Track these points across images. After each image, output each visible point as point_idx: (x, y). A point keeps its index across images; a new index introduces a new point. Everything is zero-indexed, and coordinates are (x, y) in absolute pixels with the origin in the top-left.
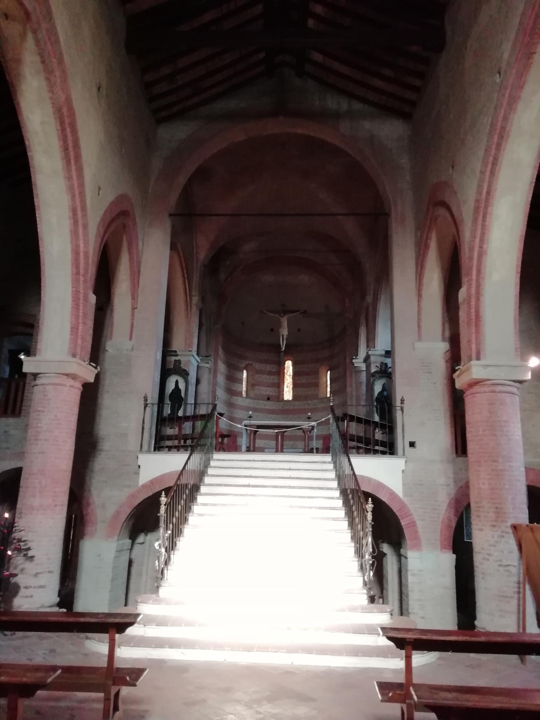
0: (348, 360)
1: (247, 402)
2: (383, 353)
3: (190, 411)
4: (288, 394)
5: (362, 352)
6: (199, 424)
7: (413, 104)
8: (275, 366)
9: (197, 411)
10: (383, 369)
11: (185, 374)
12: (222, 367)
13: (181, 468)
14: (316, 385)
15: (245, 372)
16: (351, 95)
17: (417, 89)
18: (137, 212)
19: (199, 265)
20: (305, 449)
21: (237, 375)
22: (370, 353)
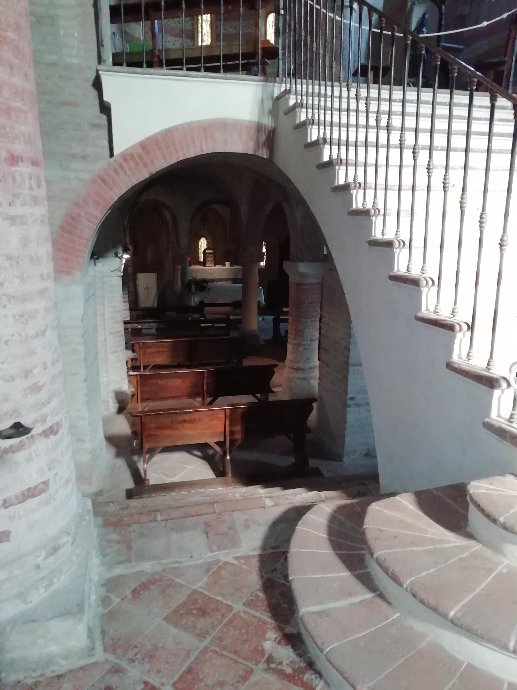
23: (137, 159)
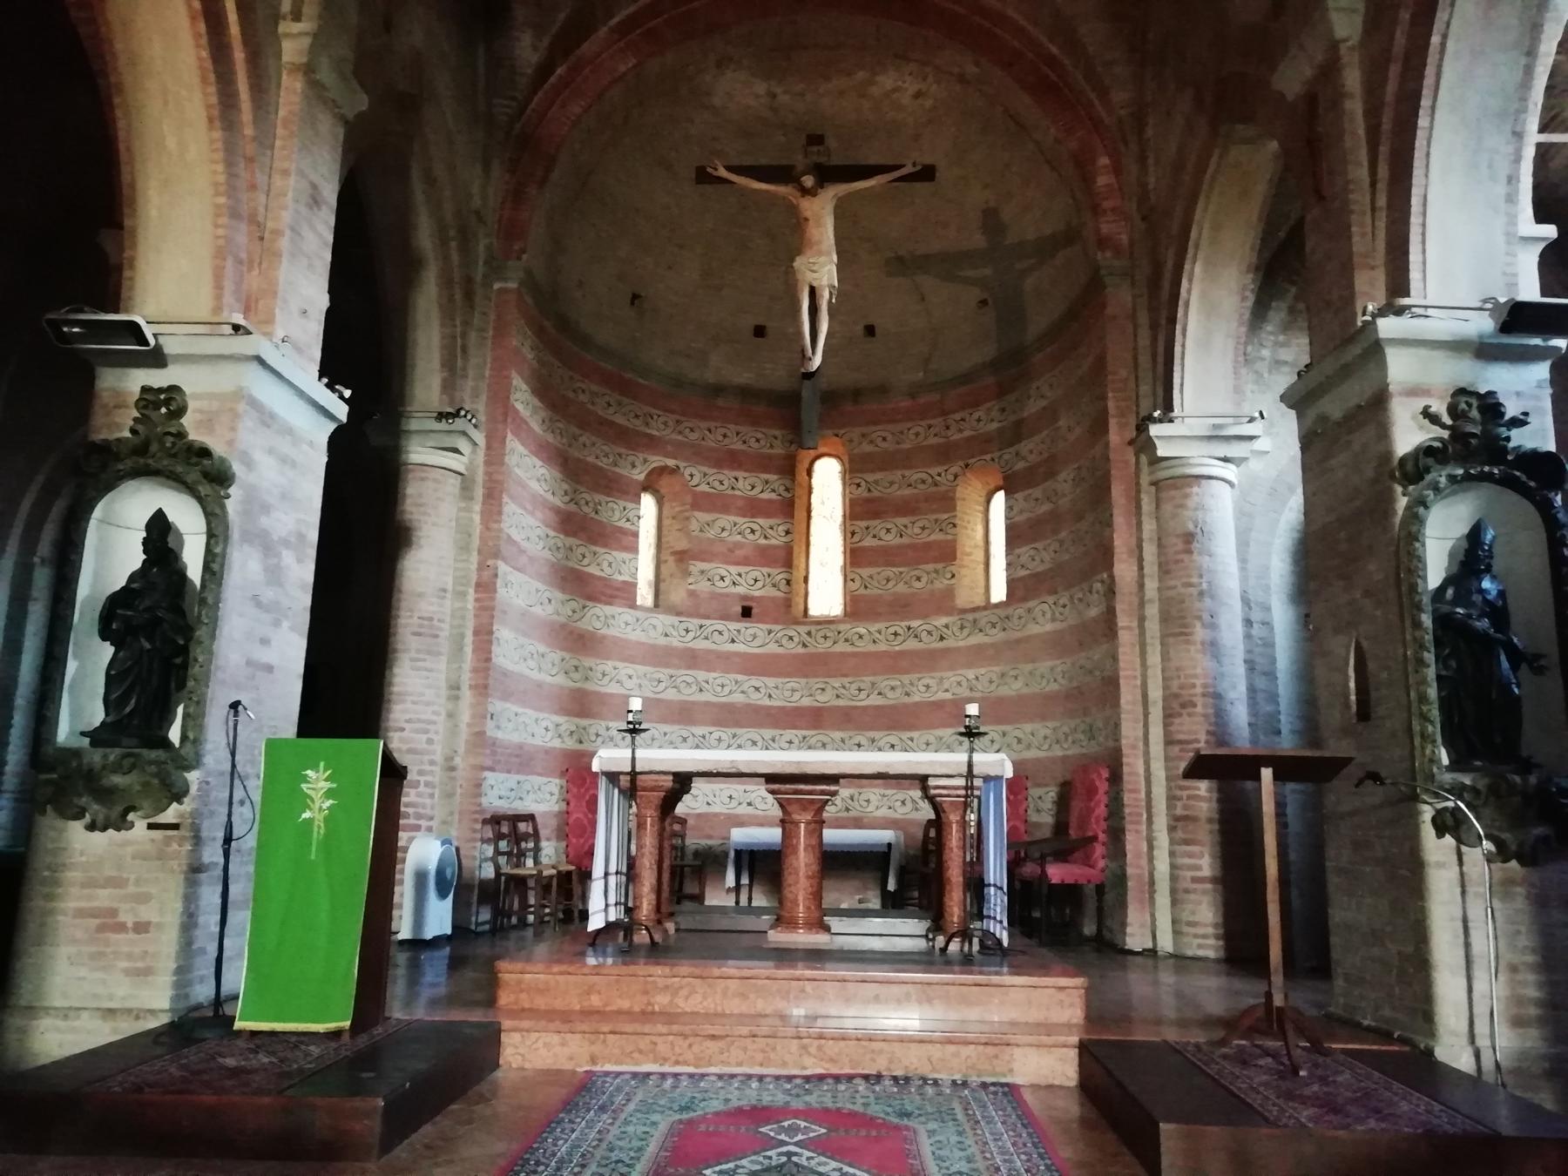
0: (1116, 435)
1: (660, 629)
2: (1483, 325)
4: (826, 592)
8: (772, 477)
12: (531, 474)
14: (947, 554)
15: (648, 503)
21: (612, 512)
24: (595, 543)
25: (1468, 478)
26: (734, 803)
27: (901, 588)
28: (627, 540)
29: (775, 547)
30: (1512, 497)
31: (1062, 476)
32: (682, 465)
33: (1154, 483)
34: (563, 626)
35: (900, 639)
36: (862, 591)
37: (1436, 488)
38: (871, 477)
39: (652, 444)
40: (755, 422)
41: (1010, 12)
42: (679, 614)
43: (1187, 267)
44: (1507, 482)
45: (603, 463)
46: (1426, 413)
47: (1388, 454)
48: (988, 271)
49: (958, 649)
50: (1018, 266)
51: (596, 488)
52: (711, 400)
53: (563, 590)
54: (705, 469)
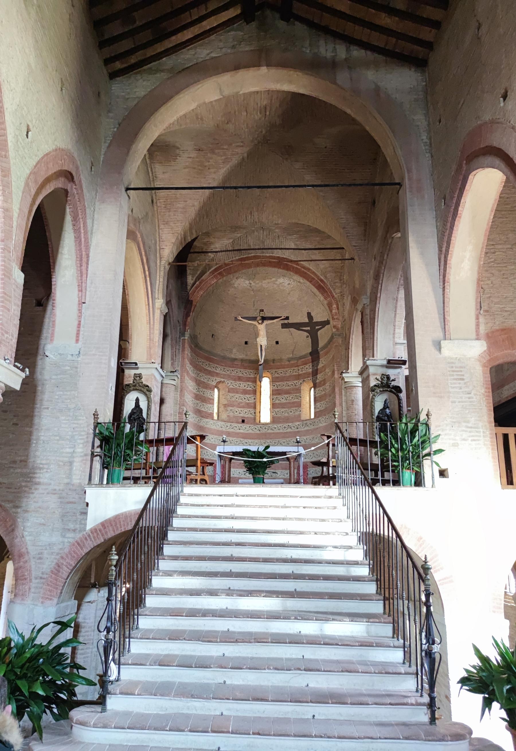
2: (385, 362)
3: (152, 435)
4: (265, 415)
5: (356, 363)
6: (166, 450)
7: (429, 46)
9: (162, 432)
10: (385, 382)
11: (146, 390)
12: (190, 385)
13: (142, 506)
14: (299, 405)
16: (350, 41)
17: (436, 25)
18: (84, 177)
19: (163, 262)
20: (290, 479)
21: (207, 393)
22: (368, 363)
23: (99, 532)
24: (203, 402)
25: (384, 391)
26: (240, 474)
27: (286, 415)
28: (210, 401)
29: (252, 403)
30: (392, 394)
31: (327, 385)
32: (225, 380)
33: (345, 388)
34: (196, 424)
35: (286, 428)
36: (275, 415)
37: (377, 393)
38: (278, 384)
39: (217, 375)
40: (245, 368)
41: (311, 268)
42: (225, 421)
43: (351, 336)
44: (391, 391)
45: (205, 381)
46: (376, 379)
47: (369, 386)
48: (309, 328)
49: (302, 431)
50: (317, 328)
51: (204, 388)
52: (232, 362)
53: (196, 415)
54: (231, 381)
